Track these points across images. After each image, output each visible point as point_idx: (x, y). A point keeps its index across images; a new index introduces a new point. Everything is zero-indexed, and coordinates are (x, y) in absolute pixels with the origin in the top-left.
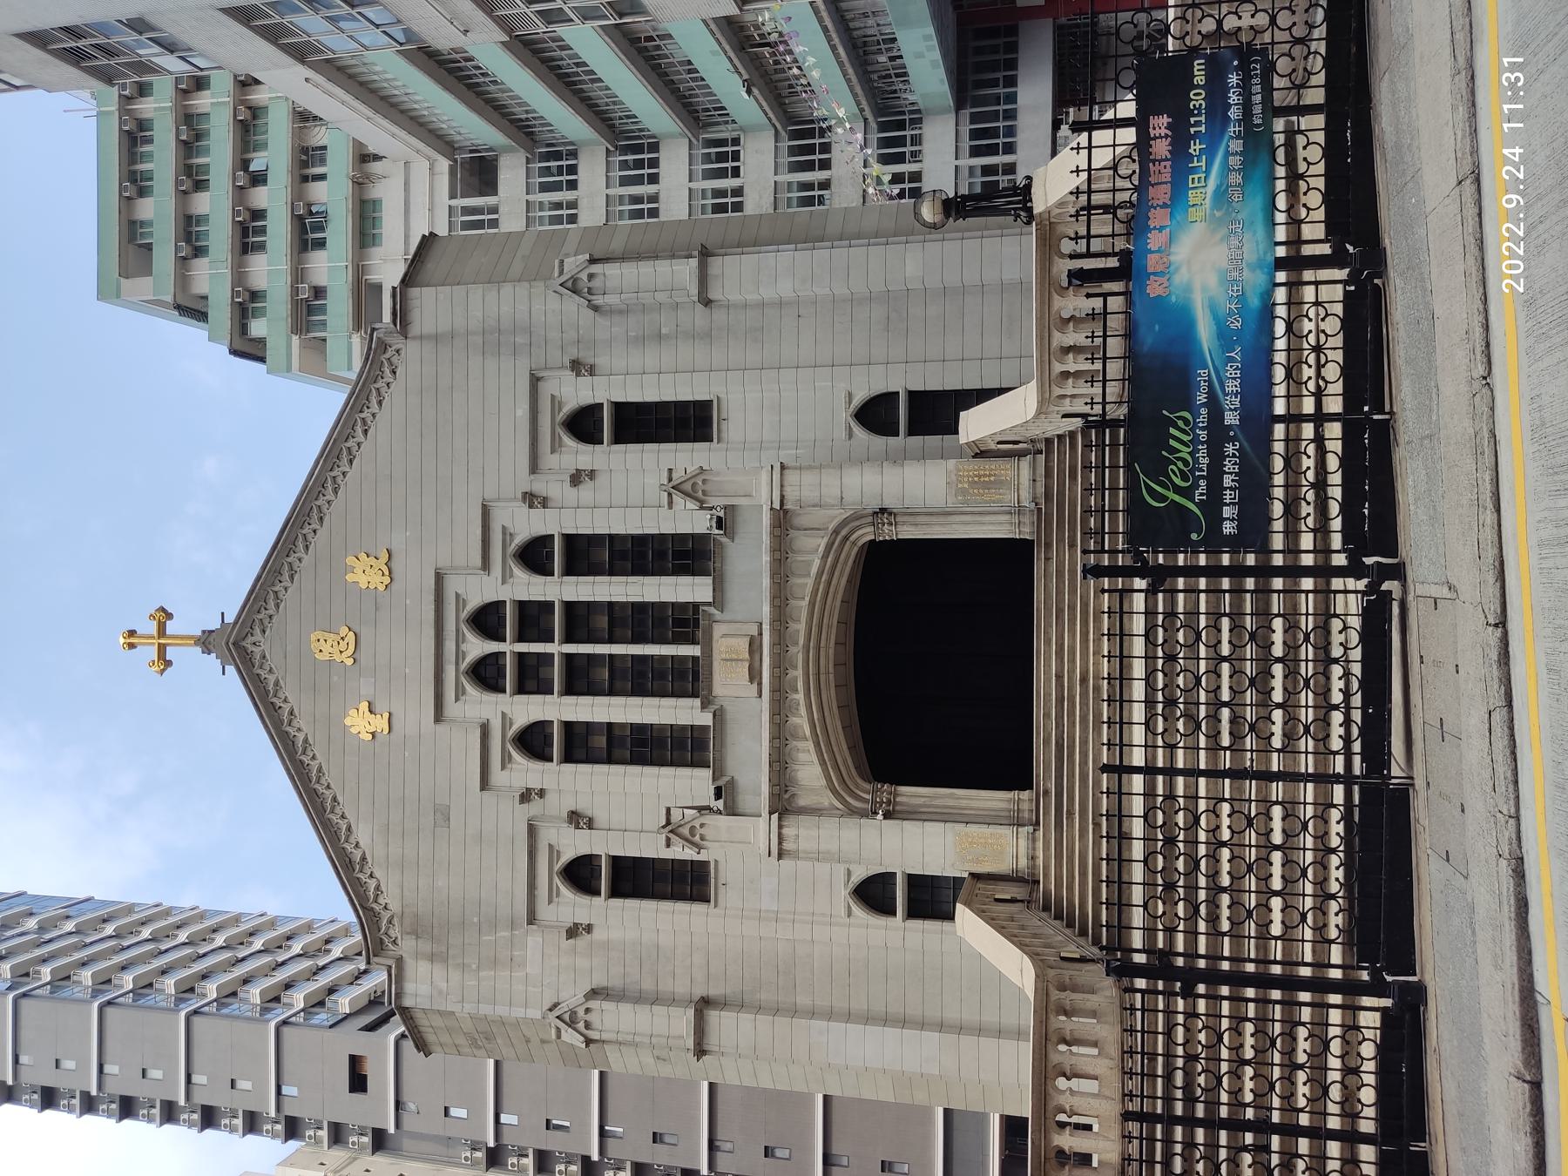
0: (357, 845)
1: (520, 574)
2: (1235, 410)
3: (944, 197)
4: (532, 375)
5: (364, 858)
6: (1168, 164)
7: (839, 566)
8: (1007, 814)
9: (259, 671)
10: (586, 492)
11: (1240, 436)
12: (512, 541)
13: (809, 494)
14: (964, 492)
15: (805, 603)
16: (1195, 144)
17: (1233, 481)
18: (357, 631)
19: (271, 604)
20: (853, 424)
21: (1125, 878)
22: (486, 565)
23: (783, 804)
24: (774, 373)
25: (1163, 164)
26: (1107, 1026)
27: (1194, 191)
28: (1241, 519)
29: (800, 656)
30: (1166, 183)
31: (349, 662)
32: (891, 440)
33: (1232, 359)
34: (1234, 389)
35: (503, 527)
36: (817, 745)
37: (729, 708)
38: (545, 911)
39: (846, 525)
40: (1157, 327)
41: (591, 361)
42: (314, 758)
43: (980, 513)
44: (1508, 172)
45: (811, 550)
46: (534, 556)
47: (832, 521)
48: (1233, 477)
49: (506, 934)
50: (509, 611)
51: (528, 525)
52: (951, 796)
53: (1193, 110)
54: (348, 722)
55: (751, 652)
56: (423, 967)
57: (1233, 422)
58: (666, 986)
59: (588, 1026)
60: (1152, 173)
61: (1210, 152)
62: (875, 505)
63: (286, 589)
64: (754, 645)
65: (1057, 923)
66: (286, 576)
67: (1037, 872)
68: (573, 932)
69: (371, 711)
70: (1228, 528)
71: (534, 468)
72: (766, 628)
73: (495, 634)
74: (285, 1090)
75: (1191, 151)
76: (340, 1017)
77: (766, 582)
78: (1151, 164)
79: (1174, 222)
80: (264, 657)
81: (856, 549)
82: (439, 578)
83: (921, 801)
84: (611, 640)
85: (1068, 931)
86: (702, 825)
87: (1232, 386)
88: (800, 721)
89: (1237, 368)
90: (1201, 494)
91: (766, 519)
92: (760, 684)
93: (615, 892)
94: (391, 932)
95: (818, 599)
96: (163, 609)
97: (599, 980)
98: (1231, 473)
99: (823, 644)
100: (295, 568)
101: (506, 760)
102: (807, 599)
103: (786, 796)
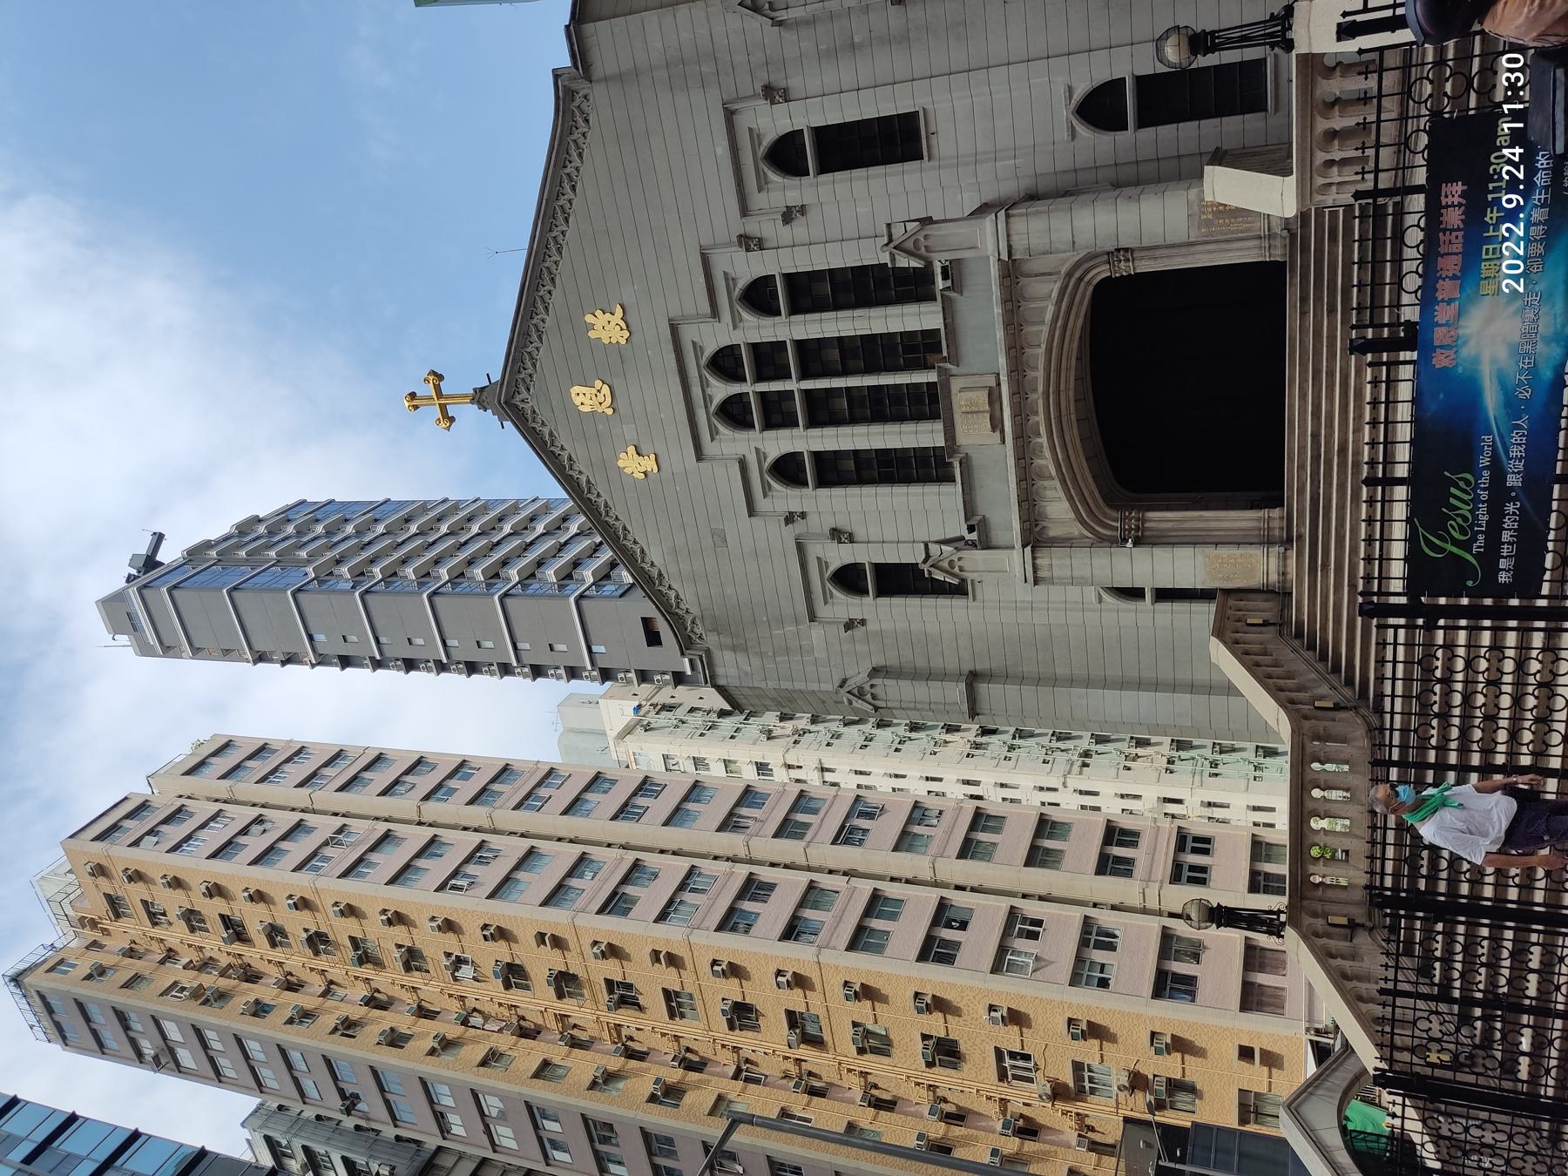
0: (652, 564)
1: (748, 317)
2: (1519, 473)
3: (1191, 32)
4: (726, 109)
5: (660, 574)
6: (1460, 234)
7: (1074, 309)
8: (1256, 532)
9: (533, 425)
10: (799, 229)
11: (1521, 496)
13: (1038, 242)
14: (1208, 223)
15: (1042, 350)
16: (1492, 212)
17: (1511, 536)
19: (528, 364)
20: (1075, 122)
21: (1377, 303)
22: (715, 313)
23: (1035, 537)
24: (983, 74)
25: (1454, 234)
26: (1358, 776)
27: (1487, 263)
28: (1517, 570)
29: (1040, 402)
30: (1456, 254)
31: (610, 412)
32: (1120, 135)
33: (1518, 427)
34: (1519, 454)
35: (725, 273)
36: (1063, 482)
37: (974, 455)
38: (822, 611)
39: (1079, 267)
40: (1442, 396)
41: (783, 84)
42: (599, 495)
43: (1227, 241)
45: (1044, 297)
46: (759, 297)
47: (1063, 264)
48: (1512, 533)
49: (793, 628)
50: (742, 346)
51: (749, 267)
52: (1200, 519)
53: (1493, 175)
54: (621, 463)
55: (991, 403)
56: (728, 656)
57: (1515, 484)
58: (937, 663)
59: (874, 697)
60: (1441, 243)
62: (1110, 246)
63: (537, 349)
64: (994, 396)
65: (1308, 655)
66: (535, 337)
67: (1288, 585)
68: (850, 625)
70: (1503, 578)
71: (745, 211)
72: (1004, 379)
74: (595, 649)
75: (1487, 219)
76: (626, 587)
77: (1000, 334)
78: (1441, 234)
79: (1464, 295)
80: (534, 412)
81: (1091, 289)
82: (674, 329)
83: (1170, 525)
84: (845, 373)
85: (1320, 666)
86: (959, 559)
87: (1515, 452)
88: (1045, 462)
89: (1523, 435)
90: (1480, 547)
92: (1002, 432)
93: (881, 592)
94: (696, 630)
95: (1055, 344)
96: (434, 373)
97: (878, 660)
98: (1510, 530)
99: (1062, 387)
100: (541, 329)
101: (766, 489)
102: (1043, 346)
103: (1037, 529)
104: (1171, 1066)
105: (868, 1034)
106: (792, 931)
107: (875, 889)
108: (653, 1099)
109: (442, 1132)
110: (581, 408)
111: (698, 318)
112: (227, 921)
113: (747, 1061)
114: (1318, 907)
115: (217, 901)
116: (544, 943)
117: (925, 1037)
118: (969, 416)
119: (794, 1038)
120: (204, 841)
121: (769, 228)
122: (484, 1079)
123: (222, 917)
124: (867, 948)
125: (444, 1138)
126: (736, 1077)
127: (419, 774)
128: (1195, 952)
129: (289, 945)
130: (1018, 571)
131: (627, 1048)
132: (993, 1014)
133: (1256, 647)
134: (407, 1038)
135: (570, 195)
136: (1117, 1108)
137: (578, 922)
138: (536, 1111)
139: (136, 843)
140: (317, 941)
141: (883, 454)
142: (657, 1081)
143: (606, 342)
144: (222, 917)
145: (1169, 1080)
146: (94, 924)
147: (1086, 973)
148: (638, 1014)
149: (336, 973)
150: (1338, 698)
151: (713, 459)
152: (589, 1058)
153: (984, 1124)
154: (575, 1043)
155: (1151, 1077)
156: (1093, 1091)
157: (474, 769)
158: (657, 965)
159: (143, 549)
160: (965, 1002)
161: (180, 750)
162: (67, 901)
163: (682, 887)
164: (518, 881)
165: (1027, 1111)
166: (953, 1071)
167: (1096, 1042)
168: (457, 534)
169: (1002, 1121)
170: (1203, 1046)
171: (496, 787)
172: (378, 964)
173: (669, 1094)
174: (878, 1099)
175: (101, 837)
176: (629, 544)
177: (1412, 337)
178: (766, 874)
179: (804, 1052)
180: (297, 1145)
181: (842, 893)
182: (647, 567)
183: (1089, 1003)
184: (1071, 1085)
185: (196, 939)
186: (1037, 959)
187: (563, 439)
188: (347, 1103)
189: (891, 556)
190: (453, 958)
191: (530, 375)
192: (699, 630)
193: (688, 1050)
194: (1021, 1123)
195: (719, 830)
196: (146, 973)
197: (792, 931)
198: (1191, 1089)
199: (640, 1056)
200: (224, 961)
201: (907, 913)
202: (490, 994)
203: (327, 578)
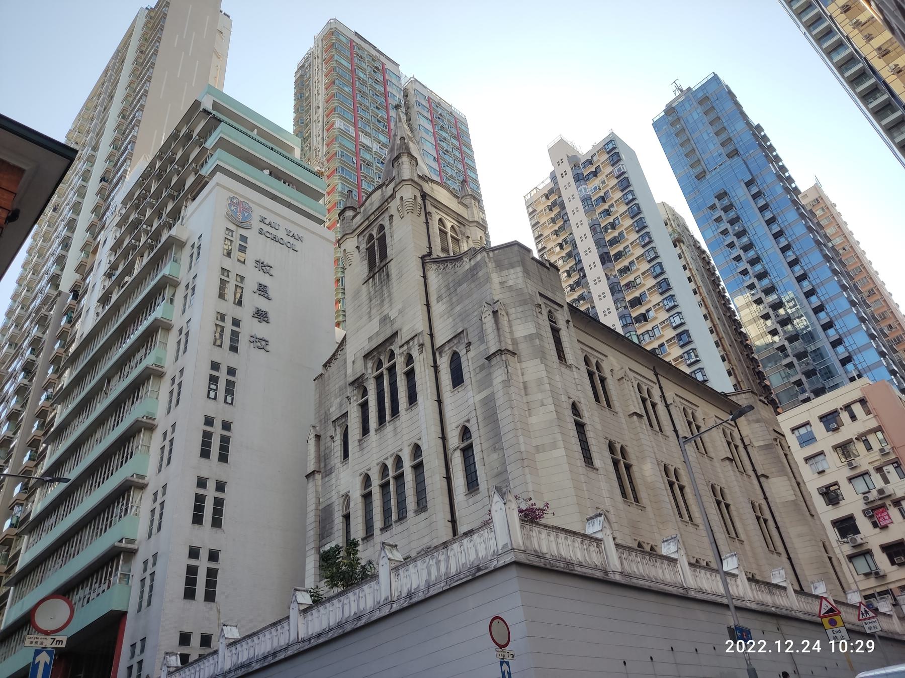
44: (806, 643)
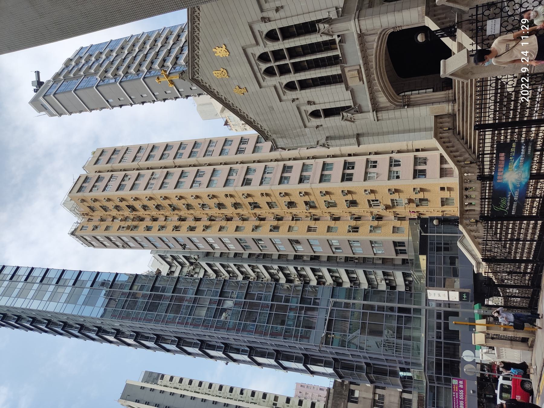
0: (251, 118)
7: (383, 42)
10: (282, 13)
12: (263, 34)
13: (370, 27)
18: (226, 69)
22: (257, 43)
23: (376, 108)
29: (375, 71)
35: (259, 31)
36: (384, 92)
42: (229, 101)
45: (373, 42)
46: (271, 36)
49: (300, 130)
51: (266, 28)
55: (359, 74)
56: (280, 140)
58: (346, 133)
59: (328, 145)
61: (515, 160)
64: (359, 72)
67: (455, 113)
68: (317, 127)
69: (240, 88)
71: (262, 10)
72: (362, 66)
73: (268, 61)
77: (359, 54)
81: (388, 35)
82: (244, 50)
85: (465, 146)
88: (378, 87)
91: (356, 36)
92: (363, 81)
97: (328, 135)
102: (374, 55)
104: (421, 195)
105: (329, 203)
106: (301, 180)
107: (324, 162)
108: (271, 230)
109: (213, 249)
110: (217, 77)
111: (251, 46)
112: (129, 207)
113: (295, 215)
114: (467, 216)
115: (124, 202)
116: (228, 197)
117: (346, 201)
118: (352, 78)
119: (308, 208)
120: (111, 186)
121: (271, 14)
122: (221, 235)
123: (127, 206)
124: (325, 181)
125: (214, 250)
126: (293, 220)
127: (169, 150)
128: (424, 161)
129: (150, 209)
130: (372, 118)
131: (259, 218)
132: (366, 192)
133: (446, 140)
134: (195, 228)
135: (198, 12)
136: (405, 208)
137: (236, 190)
138: (238, 239)
139: (91, 191)
140: (158, 207)
141: (311, 45)
142: (271, 226)
143: (222, 56)
144: (127, 206)
145: (420, 199)
146: (87, 214)
147: (392, 175)
148: (260, 209)
149: (167, 214)
150: (471, 159)
151: (265, 87)
152: (249, 223)
153: (366, 218)
154: (244, 220)
155: (414, 199)
156: (397, 205)
157: (185, 145)
158: (263, 197)
159: (34, 79)
160: (357, 190)
161: (88, 156)
162: (75, 209)
163: (264, 172)
164: (214, 180)
165: (378, 213)
166: (356, 207)
167: (397, 194)
168: (142, 51)
169: (371, 217)
170: (430, 189)
171: (195, 150)
172: (179, 210)
173: (275, 228)
174: (335, 218)
175: (79, 191)
176: (242, 114)
177: (491, 178)
178: (289, 163)
179: (312, 210)
180: (168, 255)
181: (314, 165)
182: (249, 119)
183: (394, 184)
184: (391, 205)
185: (121, 213)
186: (377, 174)
187: (214, 86)
188: (183, 247)
189: (328, 106)
190: (201, 205)
191: (198, 69)
192: (270, 134)
193: (277, 215)
194: (377, 216)
195: (270, 152)
196: (109, 225)
197: (301, 180)
198: (427, 200)
199: (263, 219)
200: (132, 217)
201: (335, 167)
202: (215, 212)
203: (104, 79)
